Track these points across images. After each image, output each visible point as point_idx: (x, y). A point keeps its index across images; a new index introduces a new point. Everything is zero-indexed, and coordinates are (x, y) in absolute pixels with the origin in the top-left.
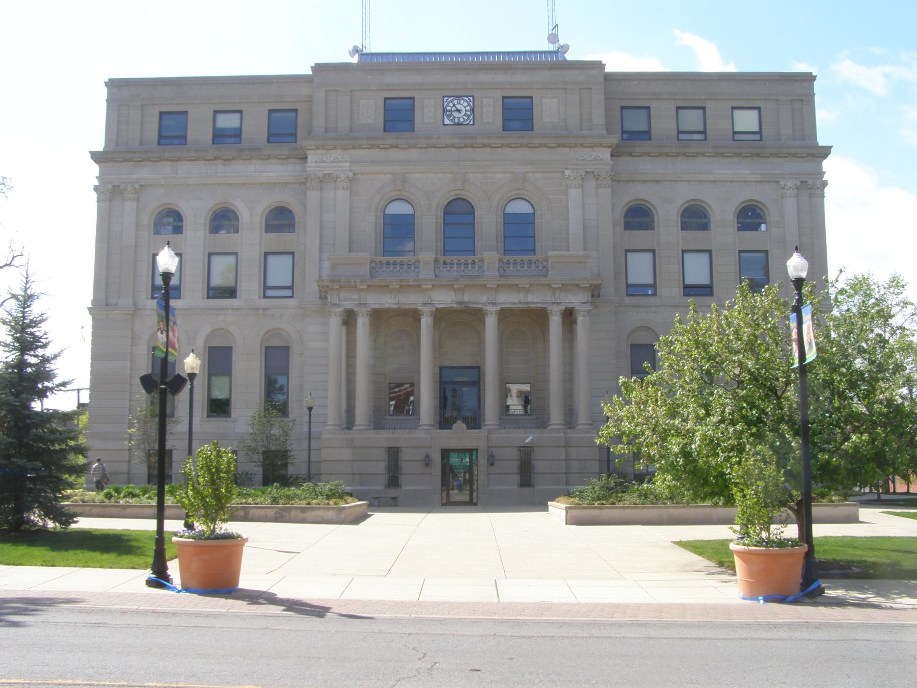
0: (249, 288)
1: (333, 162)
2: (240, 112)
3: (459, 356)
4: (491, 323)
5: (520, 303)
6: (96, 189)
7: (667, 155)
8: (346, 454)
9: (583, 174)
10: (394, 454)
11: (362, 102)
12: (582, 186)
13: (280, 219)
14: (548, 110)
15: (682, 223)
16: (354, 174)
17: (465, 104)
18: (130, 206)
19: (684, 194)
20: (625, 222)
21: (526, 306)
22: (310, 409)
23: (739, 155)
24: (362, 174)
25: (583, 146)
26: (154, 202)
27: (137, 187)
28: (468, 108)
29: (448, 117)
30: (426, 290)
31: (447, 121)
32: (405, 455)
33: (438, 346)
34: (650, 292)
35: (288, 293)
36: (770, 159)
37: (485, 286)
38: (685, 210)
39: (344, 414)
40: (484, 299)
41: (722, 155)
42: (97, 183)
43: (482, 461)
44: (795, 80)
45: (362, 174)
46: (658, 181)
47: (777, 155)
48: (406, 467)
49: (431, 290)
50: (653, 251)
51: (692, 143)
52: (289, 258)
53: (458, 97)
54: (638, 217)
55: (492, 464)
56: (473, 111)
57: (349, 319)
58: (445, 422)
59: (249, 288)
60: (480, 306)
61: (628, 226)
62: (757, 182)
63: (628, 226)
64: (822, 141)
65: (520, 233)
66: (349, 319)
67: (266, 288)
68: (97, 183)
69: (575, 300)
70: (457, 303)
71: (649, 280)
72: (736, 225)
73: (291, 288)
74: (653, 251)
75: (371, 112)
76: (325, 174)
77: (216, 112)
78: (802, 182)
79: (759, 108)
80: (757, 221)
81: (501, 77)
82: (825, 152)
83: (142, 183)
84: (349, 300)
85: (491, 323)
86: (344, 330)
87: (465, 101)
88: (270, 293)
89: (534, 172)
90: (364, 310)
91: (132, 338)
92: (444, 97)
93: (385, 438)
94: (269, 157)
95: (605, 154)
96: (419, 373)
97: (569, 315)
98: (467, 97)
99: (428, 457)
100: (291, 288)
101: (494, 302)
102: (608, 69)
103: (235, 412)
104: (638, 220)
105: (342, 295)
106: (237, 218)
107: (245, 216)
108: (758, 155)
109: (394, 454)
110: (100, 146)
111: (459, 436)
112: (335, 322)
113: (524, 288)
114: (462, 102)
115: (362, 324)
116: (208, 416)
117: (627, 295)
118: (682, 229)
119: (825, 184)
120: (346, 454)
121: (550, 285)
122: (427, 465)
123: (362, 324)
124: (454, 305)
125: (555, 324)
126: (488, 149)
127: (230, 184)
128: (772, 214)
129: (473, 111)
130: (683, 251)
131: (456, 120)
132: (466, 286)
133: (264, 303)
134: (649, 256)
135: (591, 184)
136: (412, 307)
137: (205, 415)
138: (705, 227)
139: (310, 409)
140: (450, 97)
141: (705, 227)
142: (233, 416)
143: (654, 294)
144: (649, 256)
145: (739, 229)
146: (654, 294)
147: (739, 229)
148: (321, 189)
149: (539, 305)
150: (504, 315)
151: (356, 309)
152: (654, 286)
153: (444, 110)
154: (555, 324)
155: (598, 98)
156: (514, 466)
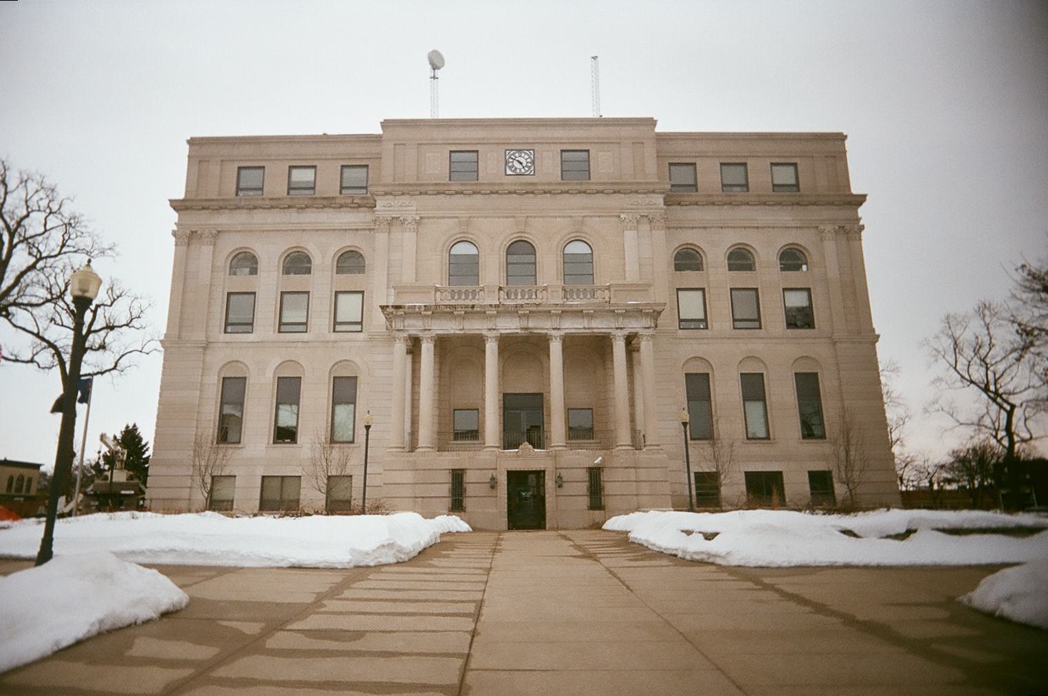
0: (320, 324)
1: (401, 206)
2: (315, 167)
3: (525, 384)
4: (556, 348)
5: (584, 328)
6: (174, 234)
7: (713, 204)
8: (408, 477)
9: (638, 217)
10: (458, 477)
11: (428, 155)
12: (636, 229)
13: (350, 261)
14: (604, 165)
15: (729, 265)
16: (421, 218)
17: (526, 157)
18: (207, 250)
19: (731, 238)
20: (675, 264)
21: (590, 331)
22: (368, 427)
23: (780, 204)
24: (428, 218)
25: (636, 192)
26: (230, 244)
27: (214, 232)
28: (529, 160)
29: (510, 168)
30: (491, 316)
31: (509, 172)
32: (469, 477)
33: (503, 374)
34: (702, 327)
35: (358, 328)
36: (809, 207)
37: (550, 312)
38: (731, 253)
39: (407, 438)
40: (548, 324)
41: (765, 204)
42: (175, 228)
43: (549, 483)
44: (828, 140)
45: (428, 218)
46: (705, 228)
47: (815, 204)
48: (471, 490)
49: (496, 317)
50: (703, 290)
51: (302, 198)
52: (361, 295)
53: (520, 151)
54: (687, 259)
55: (560, 486)
56: (533, 162)
57: (414, 346)
58: (509, 443)
59: (320, 324)
60: (544, 331)
61: (678, 268)
62: (797, 228)
63: (678, 268)
64: (855, 190)
65: (578, 270)
66: (414, 346)
67: (335, 323)
68: (175, 228)
69: (634, 325)
70: (522, 329)
71: (702, 316)
72: (779, 266)
73: (361, 323)
74: (703, 290)
75: (436, 166)
76: (393, 218)
77: (291, 167)
78: (839, 227)
79: (795, 165)
80: (800, 262)
81: (560, 133)
82: (860, 200)
83: (219, 229)
84: (415, 326)
85: (556, 348)
86: (409, 357)
87: (526, 154)
88: (338, 328)
89: (591, 217)
90: (494, 333)
91: (203, 369)
92: (506, 150)
93: (451, 460)
94: (341, 206)
95: (659, 200)
96: (484, 400)
97: (631, 342)
98: (528, 150)
99: (493, 479)
100: (361, 323)
101: (557, 330)
102: (658, 129)
103: (300, 438)
104: (687, 262)
105: (407, 322)
106: (309, 261)
107: (317, 260)
108: (798, 204)
109: (458, 477)
110: (181, 195)
111: (527, 458)
112: (400, 347)
113: (588, 315)
114: (523, 155)
115: (427, 349)
116: (274, 443)
117: (680, 329)
118: (729, 270)
119: (862, 228)
120: (408, 477)
121: (613, 311)
122: (493, 487)
123: (427, 349)
124: (519, 331)
125: (619, 349)
126: (548, 195)
127: (304, 230)
128: (813, 254)
129: (533, 162)
130: (784, 289)
131: (518, 171)
132: (530, 312)
133: (334, 336)
134: (341, 297)
135: (645, 227)
136: (477, 332)
137: (271, 441)
138: (750, 267)
139: (368, 427)
140: (512, 150)
141: (750, 267)
142: (298, 442)
143: (706, 328)
144: (700, 293)
145: (782, 269)
146: (706, 328)
147: (782, 269)
148: (389, 233)
149: (603, 331)
150: (570, 343)
151: (420, 334)
152: (705, 320)
153: (506, 163)
154: (619, 349)
155: (650, 151)
156: (583, 488)
